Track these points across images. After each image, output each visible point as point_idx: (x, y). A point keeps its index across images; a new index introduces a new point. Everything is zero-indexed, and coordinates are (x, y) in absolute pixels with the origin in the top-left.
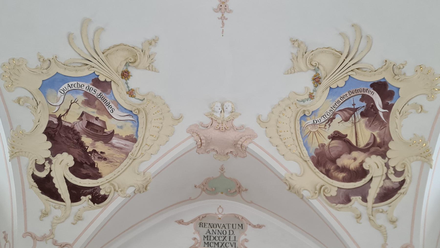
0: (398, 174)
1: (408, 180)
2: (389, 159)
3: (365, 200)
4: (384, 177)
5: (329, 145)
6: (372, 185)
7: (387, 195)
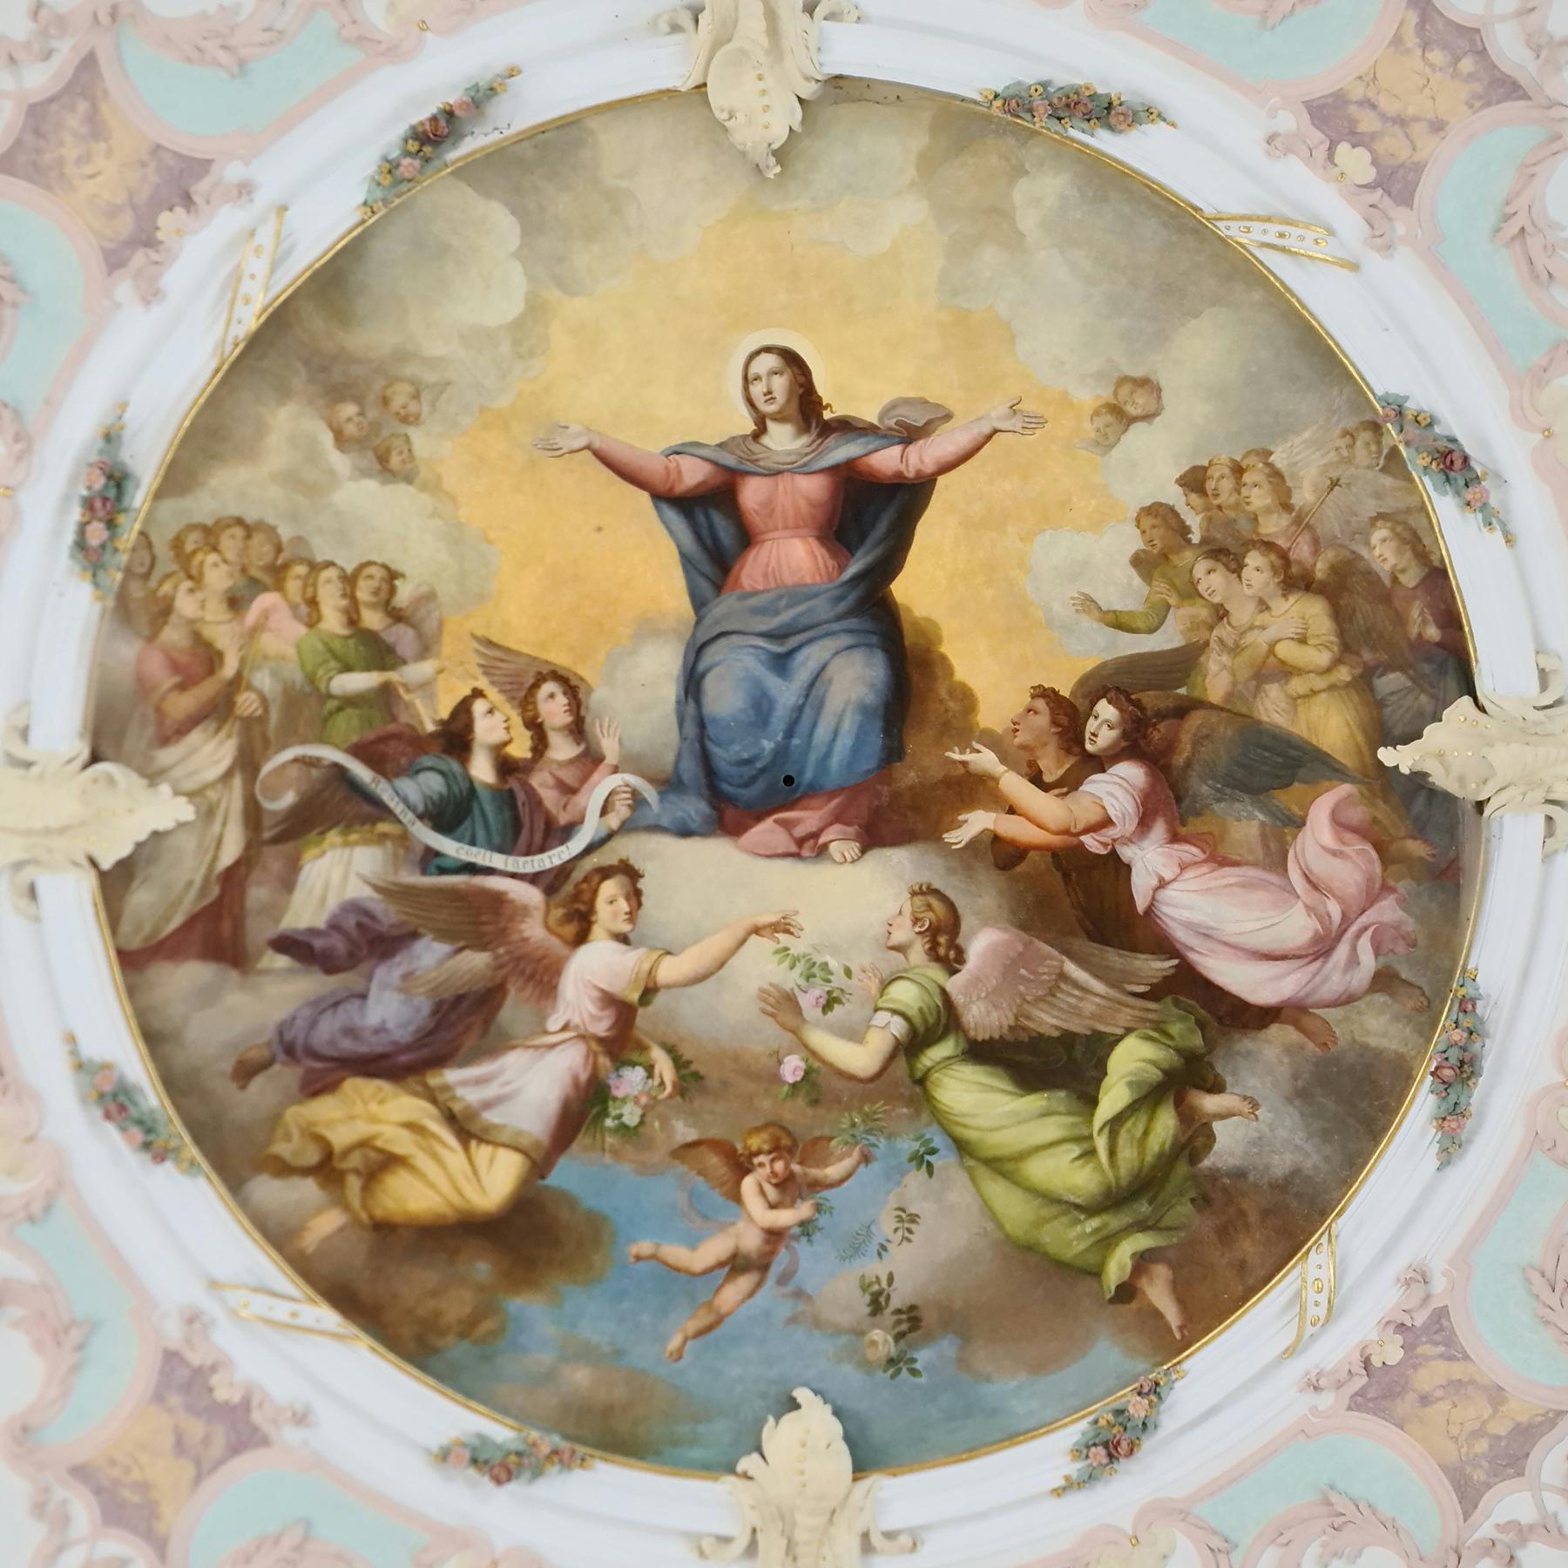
5: (706, 759)
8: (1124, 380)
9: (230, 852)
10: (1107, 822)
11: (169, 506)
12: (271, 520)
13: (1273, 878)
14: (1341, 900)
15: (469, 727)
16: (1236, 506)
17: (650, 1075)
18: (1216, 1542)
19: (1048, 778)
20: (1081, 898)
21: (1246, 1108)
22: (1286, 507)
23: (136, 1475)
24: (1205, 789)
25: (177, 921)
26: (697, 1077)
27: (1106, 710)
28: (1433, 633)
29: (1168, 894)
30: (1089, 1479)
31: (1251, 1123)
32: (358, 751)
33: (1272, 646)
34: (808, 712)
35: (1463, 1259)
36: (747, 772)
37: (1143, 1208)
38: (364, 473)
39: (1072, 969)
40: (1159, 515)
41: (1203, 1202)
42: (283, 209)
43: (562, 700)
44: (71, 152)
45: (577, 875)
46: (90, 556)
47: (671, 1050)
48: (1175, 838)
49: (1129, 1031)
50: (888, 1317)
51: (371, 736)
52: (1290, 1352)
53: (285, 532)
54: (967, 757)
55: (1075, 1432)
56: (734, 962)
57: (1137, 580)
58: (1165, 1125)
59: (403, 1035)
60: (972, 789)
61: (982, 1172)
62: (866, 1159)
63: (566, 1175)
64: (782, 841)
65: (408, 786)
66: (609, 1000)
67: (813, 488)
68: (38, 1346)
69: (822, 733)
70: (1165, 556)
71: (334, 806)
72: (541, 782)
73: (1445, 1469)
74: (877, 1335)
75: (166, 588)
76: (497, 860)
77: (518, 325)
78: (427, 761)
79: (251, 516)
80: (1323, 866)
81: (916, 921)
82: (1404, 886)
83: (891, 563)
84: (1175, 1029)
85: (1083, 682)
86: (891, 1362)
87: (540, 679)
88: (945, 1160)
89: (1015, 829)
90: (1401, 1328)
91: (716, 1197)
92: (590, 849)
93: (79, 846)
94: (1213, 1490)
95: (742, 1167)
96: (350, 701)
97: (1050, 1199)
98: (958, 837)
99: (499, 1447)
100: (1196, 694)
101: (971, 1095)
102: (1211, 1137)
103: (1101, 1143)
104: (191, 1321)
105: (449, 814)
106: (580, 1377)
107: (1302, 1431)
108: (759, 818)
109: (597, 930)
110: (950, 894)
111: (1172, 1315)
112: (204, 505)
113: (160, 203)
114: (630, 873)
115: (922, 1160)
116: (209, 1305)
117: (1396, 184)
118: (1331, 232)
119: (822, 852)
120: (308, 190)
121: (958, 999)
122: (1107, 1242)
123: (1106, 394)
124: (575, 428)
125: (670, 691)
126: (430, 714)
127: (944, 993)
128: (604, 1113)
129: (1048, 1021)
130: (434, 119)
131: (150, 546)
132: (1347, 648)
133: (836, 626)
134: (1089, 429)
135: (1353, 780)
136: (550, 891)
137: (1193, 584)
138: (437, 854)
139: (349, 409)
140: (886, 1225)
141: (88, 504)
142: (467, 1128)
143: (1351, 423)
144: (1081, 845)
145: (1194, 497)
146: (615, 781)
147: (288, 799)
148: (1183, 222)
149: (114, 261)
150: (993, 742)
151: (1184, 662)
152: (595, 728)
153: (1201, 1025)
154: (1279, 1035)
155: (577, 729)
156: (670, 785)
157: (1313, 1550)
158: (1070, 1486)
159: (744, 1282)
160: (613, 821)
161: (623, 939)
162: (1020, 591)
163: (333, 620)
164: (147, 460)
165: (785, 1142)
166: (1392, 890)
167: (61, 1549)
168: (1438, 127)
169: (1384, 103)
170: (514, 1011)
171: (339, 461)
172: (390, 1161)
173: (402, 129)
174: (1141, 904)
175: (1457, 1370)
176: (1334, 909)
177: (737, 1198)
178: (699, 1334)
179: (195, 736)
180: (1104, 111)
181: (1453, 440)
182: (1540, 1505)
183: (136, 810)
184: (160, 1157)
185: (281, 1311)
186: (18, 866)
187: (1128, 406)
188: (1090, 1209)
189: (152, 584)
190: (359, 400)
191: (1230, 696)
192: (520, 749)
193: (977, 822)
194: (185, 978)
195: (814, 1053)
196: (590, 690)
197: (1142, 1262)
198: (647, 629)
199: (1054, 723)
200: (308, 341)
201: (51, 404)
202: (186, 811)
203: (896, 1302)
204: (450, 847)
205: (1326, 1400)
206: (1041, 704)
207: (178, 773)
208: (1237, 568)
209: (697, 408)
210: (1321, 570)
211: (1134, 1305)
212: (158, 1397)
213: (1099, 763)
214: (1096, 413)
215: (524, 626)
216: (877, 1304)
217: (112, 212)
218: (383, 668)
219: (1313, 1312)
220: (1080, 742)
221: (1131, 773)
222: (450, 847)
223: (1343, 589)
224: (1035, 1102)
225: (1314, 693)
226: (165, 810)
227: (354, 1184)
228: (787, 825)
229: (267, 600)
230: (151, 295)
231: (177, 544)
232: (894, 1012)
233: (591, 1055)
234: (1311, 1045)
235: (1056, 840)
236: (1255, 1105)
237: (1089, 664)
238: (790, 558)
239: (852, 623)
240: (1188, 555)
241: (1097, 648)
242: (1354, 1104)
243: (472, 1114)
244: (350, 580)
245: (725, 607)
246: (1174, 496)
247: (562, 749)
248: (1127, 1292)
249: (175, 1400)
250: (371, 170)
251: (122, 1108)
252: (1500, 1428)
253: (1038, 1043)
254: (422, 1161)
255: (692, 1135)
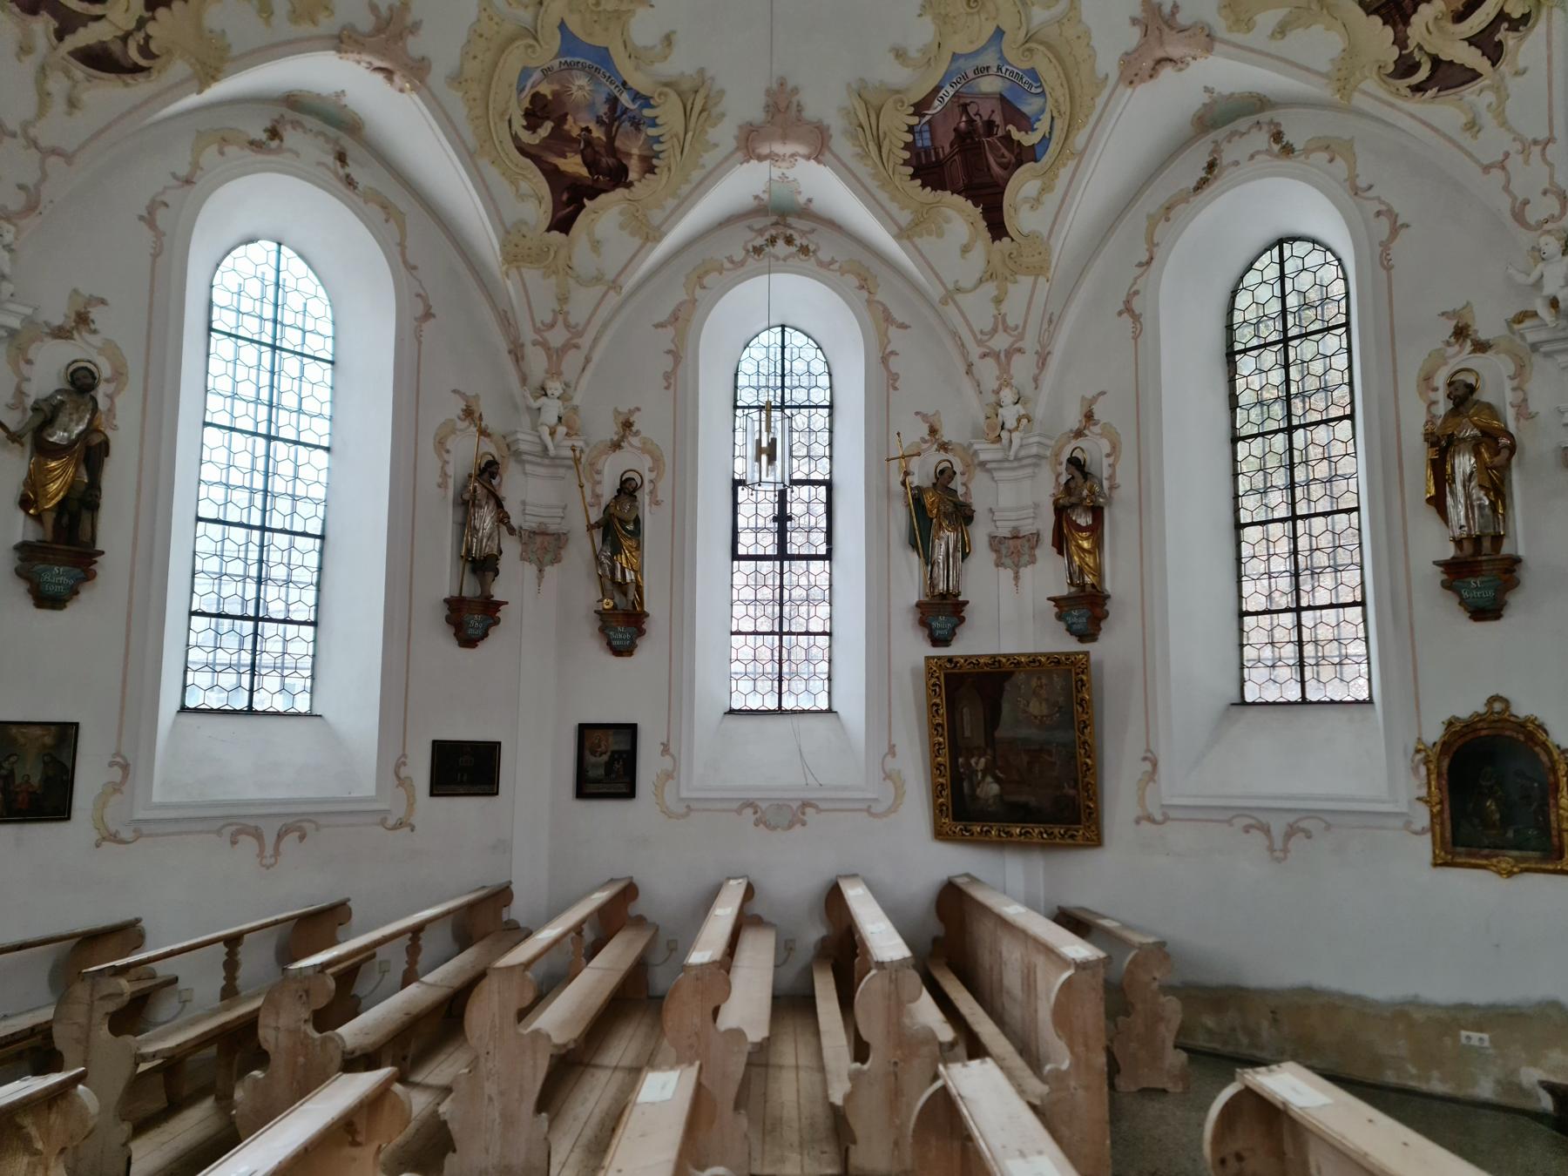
0: (145, 51)
1: (154, 74)
2: (153, 18)
3: (60, 35)
4: (120, 33)
6: (93, 26)
7: (100, 60)
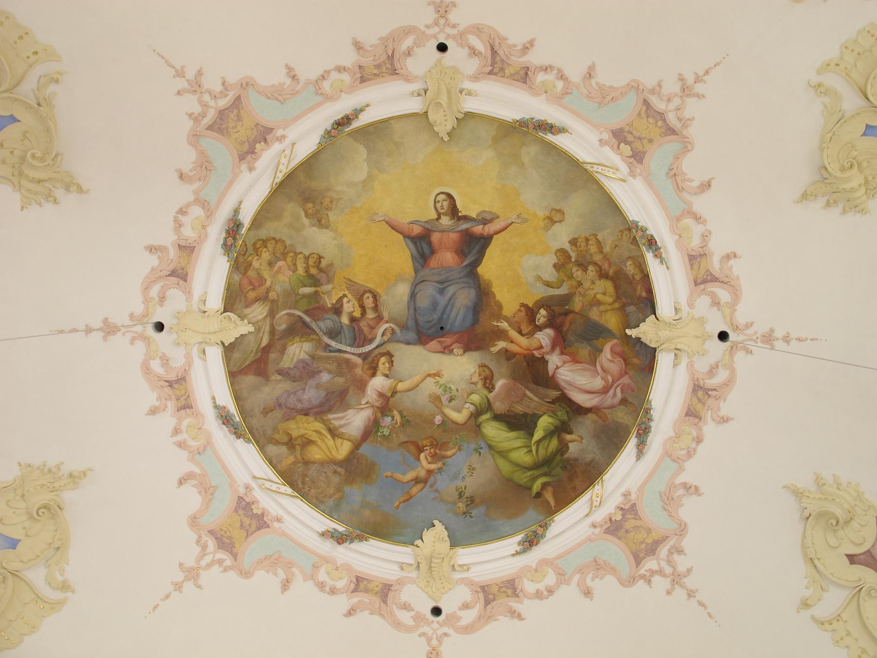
5: (417, 323)
8: (553, 209)
9: (265, 342)
10: (541, 347)
11: (252, 233)
12: (283, 239)
13: (592, 368)
14: (612, 376)
15: (342, 306)
16: (586, 251)
17: (393, 419)
18: (561, 572)
19: (524, 332)
20: (533, 371)
21: (579, 439)
22: (601, 252)
23: (228, 534)
24: (572, 339)
25: (247, 363)
26: (408, 421)
27: (543, 312)
28: (644, 294)
29: (560, 371)
30: (524, 551)
31: (580, 444)
32: (306, 312)
33: (595, 295)
34: (449, 307)
35: (641, 489)
36: (429, 325)
37: (545, 469)
38: (313, 225)
39: (528, 393)
40: (562, 252)
41: (564, 468)
42: (294, 144)
43: (371, 299)
44: (231, 125)
45: (373, 355)
46: (227, 247)
47: (400, 412)
48: (562, 353)
49: (545, 413)
50: (464, 499)
51: (311, 307)
52: (587, 515)
53: (288, 243)
54: (499, 324)
55: (519, 537)
56: (422, 385)
57: (555, 272)
58: (554, 443)
59: (316, 402)
60: (501, 334)
61: (496, 456)
62: (460, 449)
63: (364, 449)
64: (439, 347)
65: (321, 324)
66: (381, 395)
67: (454, 236)
68: (200, 492)
69: (453, 314)
70: (563, 265)
71: (298, 329)
72: (363, 324)
73: (632, 553)
74: (460, 505)
75: (250, 258)
76: (348, 349)
77: (364, 181)
78: (327, 316)
79: (278, 237)
80: (607, 364)
81: (480, 375)
82: (632, 373)
83: (477, 262)
84: (559, 413)
85: (536, 303)
86: (464, 513)
87: (365, 292)
88: (485, 451)
89: (514, 348)
90: (621, 509)
91: (412, 459)
92: (377, 347)
93: (217, 338)
94: (561, 556)
95: (420, 450)
96: (304, 296)
97: (517, 465)
98: (494, 349)
99: (340, 533)
100: (571, 308)
101: (493, 431)
102: (568, 448)
103: (534, 448)
104: (247, 488)
105: (334, 334)
106: (367, 513)
107: (589, 539)
108: (432, 340)
109: (379, 373)
110: (491, 367)
111: (552, 503)
112: (263, 233)
113: (257, 141)
114: (390, 355)
115: (477, 450)
116: (253, 484)
117: (638, 157)
118: (617, 170)
119: (451, 352)
120: (302, 139)
121: (492, 400)
122: (534, 479)
123: (547, 213)
124: (380, 214)
125: (406, 298)
126: (329, 302)
127: (488, 400)
128: (378, 431)
129: (519, 409)
130: (342, 118)
131: (246, 245)
132: (618, 298)
133: (459, 281)
134: (541, 224)
135: (618, 339)
136: (364, 359)
137: (572, 274)
138: (329, 346)
139: (310, 205)
140: (465, 471)
141: (228, 232)
142: (334, 433)
143: (622, 228)
144: (533, 354)
145: (573, 247)
146: (387, 325)
147: (284, 326)
148: (575, 164)
149: (242, 158)
150: (506, 319)
151: (566, 299)
152: (381, 308)
153: (567, 412)
154: (591, 416)
155: (376, 308)
156: (404, 327)
157: (590, 575)
158: (517, 553)
159: (420, 486)
160: (386, 338)
161: (387, 376)
162: (518, 272)
163: (301, 270)
164: (246, 217)
165: (435, 443)
166: (628, 373)
167: (205, 555)
168: (651, 141)
169: (635, 133)
170: (351, 397)
171: (306, 221)
172: (311, 442)
173: (332, 121)
174: (550, 374)
175: (638, 523)
176: (610, 379)
177: (418, 459)
178: (404, 501)
179: (256, 305)
180: (551, 128)
181: (652, 236)
182: (659, 565)
183: (237, 328)
184: (238, 437)
185: (274, 487)
186: (201, 343)
187: (554, 218)
188: (528, 469)
189: (246, 257)
190: (313, 202)
191: (582, 310)
192: (357, 314)
193: (501, 345)
194: (250, 379)
195: (445, 415)
196: (380, 297)
197: (544, 486)
198: (400, 278)
199: (527, 315)
200: (301, 188)
201: (219, 201)
202: (251, 329)
203: (467, 495)
204: (333, 344)
205: (597, 531)
206: (523, 309)
207: (250, 316)
208: (585, 270)
209: (419, 210)
210: (611, 272)
211: (541, 499)
212: (236, 511)
213: (540, 328)
214: (544, 219)
215: (363, 277)
216: (460, 496)
217: (242, 143)
218: (315, 286)
219: (595, 504)
220: (535, 321)
221: (549, 332)
222: (333, 344)
223: (618, 279)
224: (514, 434)
225: (607, 311)
226: (245, 328)
227: (298, 448)
228: (440, 342)
229: (281, 263)
230: (251, 169)
231: (254, 244)
232: (472, 404)
233: (375, 413)
234: (600, 421)
235: (525, 352)
236: (582, 439)
237: (539, 297)
238: (447, 258)
239: (465, 280)
240: (571, 265)
241: (540, 292)
242: (612, 440)
243: (336, 428)
244: (307, 258)
245: (425, 272)
246: (567, 246)
247: (370, 315)
248: (539, 495)
249: (241, 512)
250: (322, 133)
251: (228, 421)
252: (649, 541)
253: (516, 416)
254: (319, 442)
255: (406, 439)
